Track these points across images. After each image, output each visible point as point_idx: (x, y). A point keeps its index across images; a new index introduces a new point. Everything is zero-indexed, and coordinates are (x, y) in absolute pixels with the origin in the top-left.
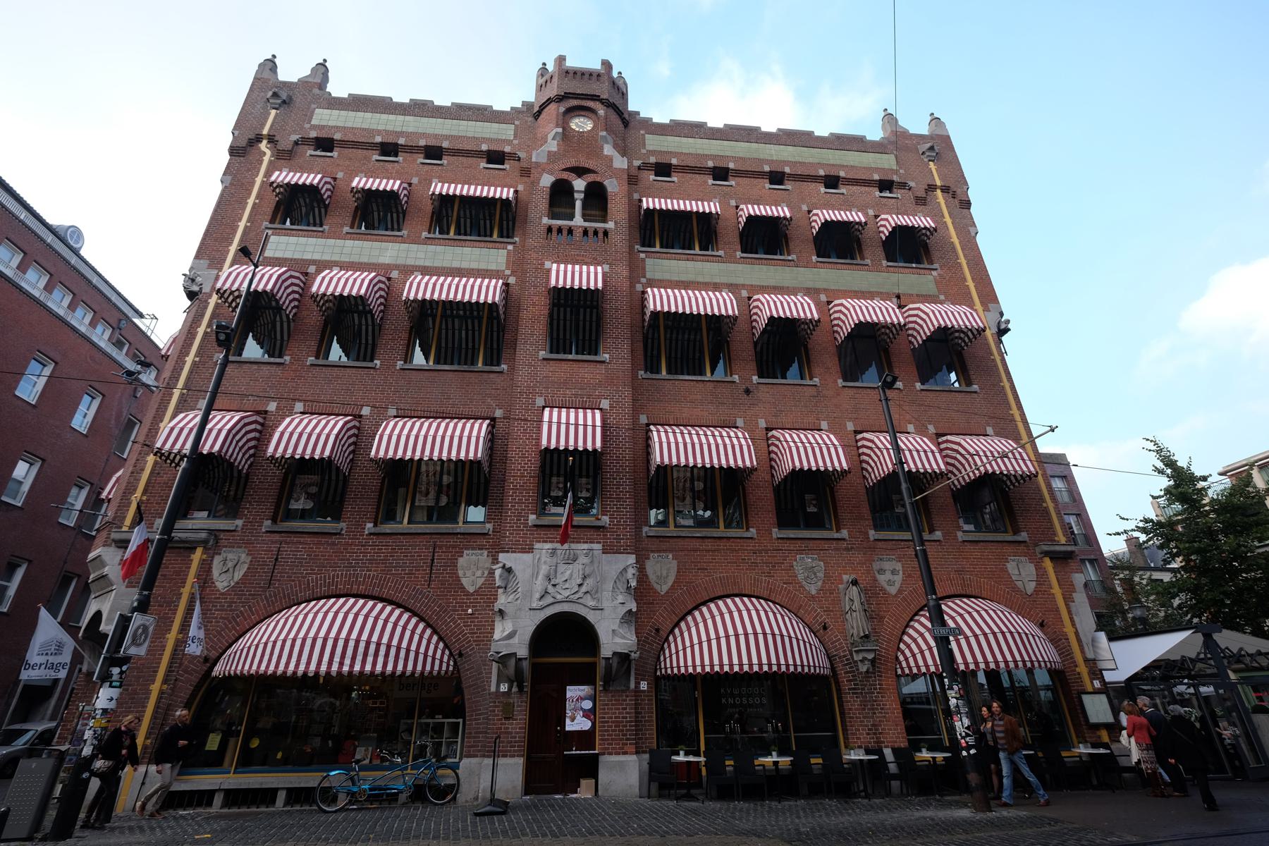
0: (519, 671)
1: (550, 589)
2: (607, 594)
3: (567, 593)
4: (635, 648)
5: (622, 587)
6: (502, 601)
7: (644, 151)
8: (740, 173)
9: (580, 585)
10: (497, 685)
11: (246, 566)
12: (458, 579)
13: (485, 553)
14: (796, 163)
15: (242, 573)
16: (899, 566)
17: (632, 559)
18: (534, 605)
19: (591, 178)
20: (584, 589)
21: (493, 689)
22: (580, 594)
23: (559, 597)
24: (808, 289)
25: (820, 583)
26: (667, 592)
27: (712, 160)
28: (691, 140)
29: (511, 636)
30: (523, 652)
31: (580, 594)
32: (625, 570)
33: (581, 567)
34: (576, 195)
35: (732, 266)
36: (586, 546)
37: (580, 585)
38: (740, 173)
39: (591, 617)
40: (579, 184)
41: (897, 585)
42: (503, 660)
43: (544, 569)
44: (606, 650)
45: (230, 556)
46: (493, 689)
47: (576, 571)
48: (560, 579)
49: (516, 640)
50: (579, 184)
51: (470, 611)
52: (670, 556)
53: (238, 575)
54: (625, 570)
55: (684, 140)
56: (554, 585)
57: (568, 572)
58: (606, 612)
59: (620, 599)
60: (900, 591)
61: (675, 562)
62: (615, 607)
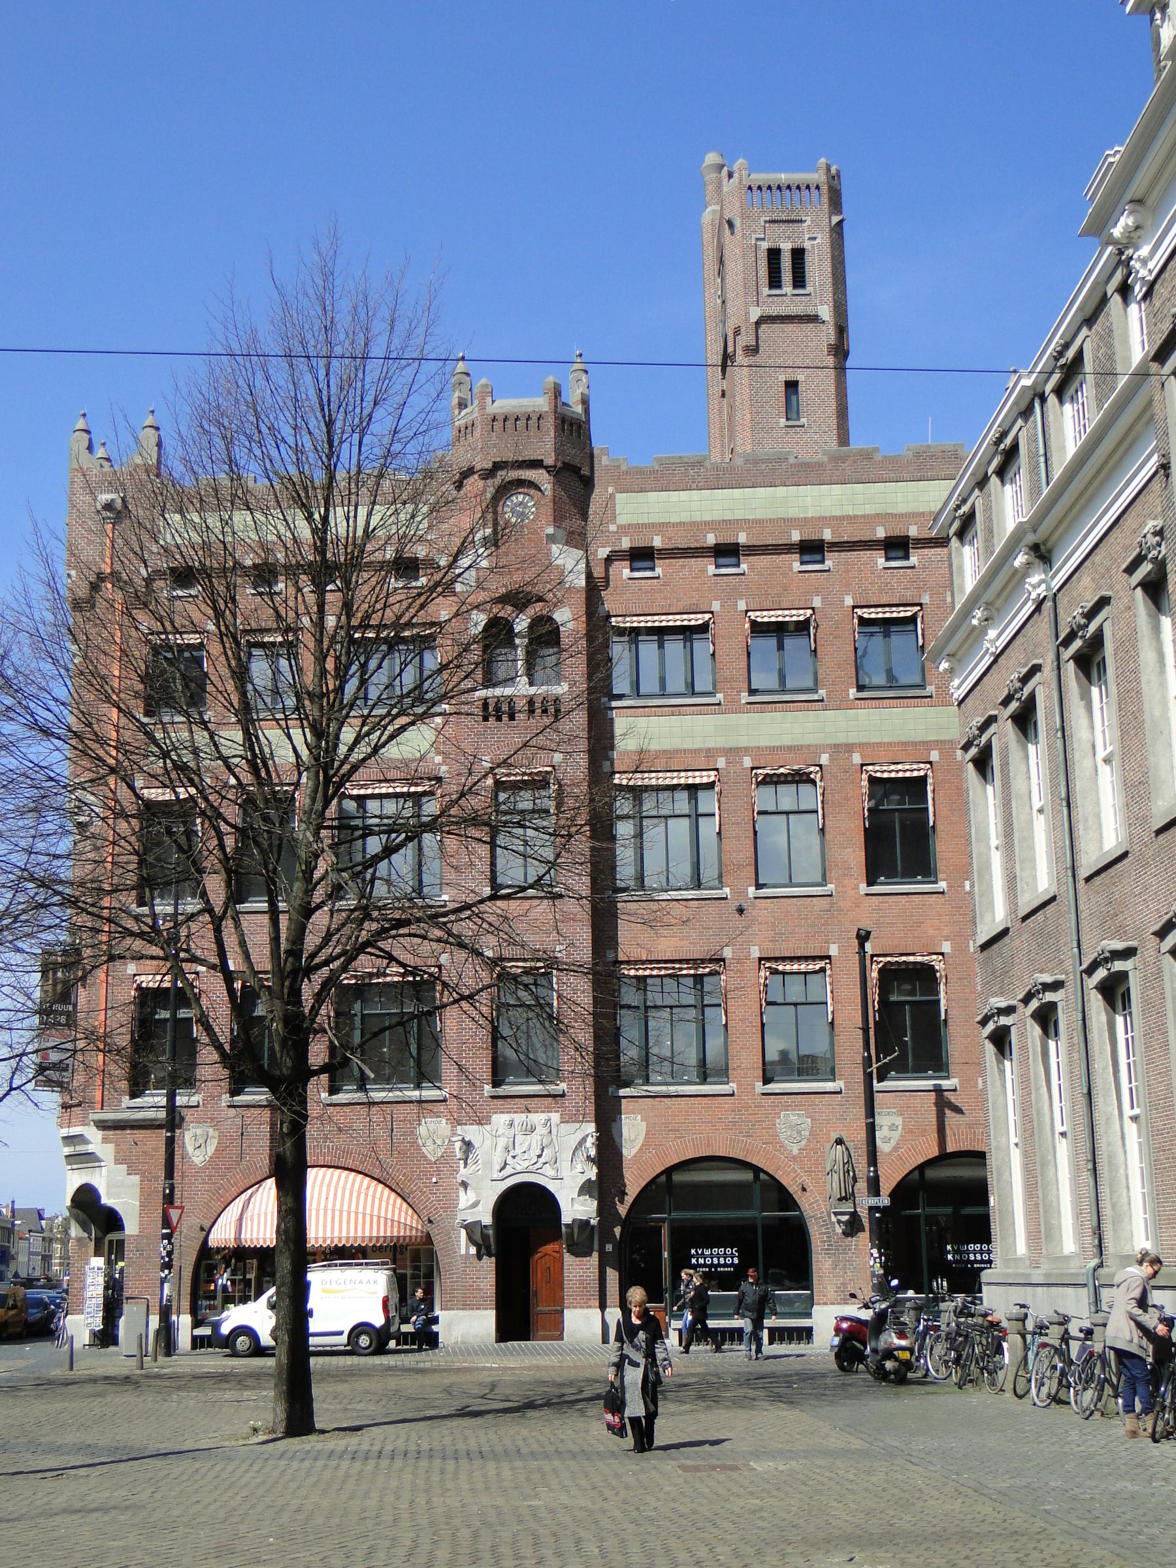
0: (485, 1237)
1: (510, 1160)
2: (564, 1165)
3: (526, 1164)
4: (595, 1215)
5: (581, 1156)
6: (463, 1173)
7: (613, 528)
8: (754, 550)
9: (539, 1156)
10: (464, 1246)
11: (216, 1141)
12: (418, 1148)
13: (444, 1121)
14: (842, 518)
15: (213, 1148)
16: (899, 1121)
17: (591, 1128)
18: (496, 1175)
19: (536, 609)
20: (542, 1160)
21: (463, 1252)
22: (538, 1165)
23: (519, 1168)
24: (836, 746)
25: (803, 1143)
26: (635, 1156)
27: (714, 530)
28: (684, 495)
29: (475, 1205)
30: (487, 1220)
31: (538, 1165)
32: (584, 1140)
33: (539, 1138)
34: (517, 641)
35: (733, 718)
36: (543, 1117)
37: (539, 1156)
38: (754, 550)
39: (551, 1186)
40: (521, 624)
41: (893, 1142)
42: (470, 1228)
43: (502, 1142)
44: (566, 1219)
45: (199, 1131)
46: (463, 1252)
47: (534, 1142)
48: (518, 1151)
49: (480, 1207)
50: (521, 624)
51: (434, 1180)
52: (639, 1117)
53: (211, 1149)
54: (584, 1140)
55: (674, 496)
56: (514, 1157)
57: (527, 1143)
58: (565, 1181)
59: (579, 1168)
60: (895, 1149)
61: (644, 1124)
62: (574, 1177)
